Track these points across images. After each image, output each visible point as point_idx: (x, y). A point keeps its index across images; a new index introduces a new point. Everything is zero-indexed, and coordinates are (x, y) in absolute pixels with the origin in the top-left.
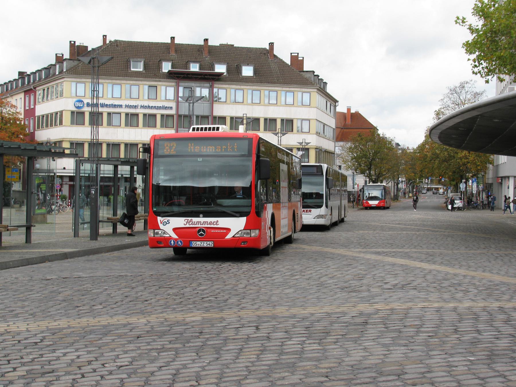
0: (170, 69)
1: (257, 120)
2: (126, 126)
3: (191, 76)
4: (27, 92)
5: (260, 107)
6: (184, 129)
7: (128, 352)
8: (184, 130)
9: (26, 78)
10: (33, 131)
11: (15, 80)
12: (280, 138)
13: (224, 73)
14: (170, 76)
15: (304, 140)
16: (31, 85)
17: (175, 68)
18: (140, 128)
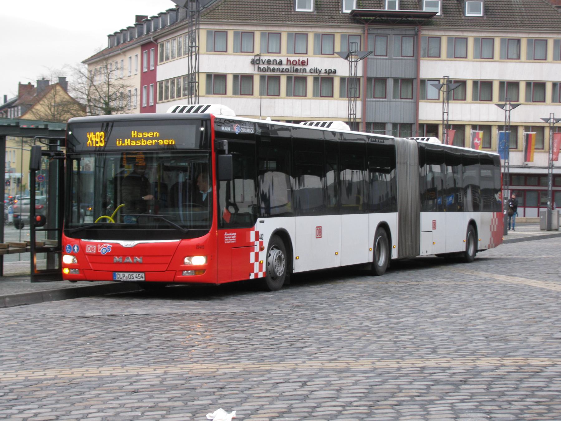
0: (354, 8)
1: (462, 83)
2: (287, 95)
3: (386, 18)
4: (146, 46)
5: (493, 63)
6: (374, 99)
7: (105, 411)
8: (375, 101)
9: (145, 26)
10: (153, 104)
11: (129, 28)
12: (508, 112)
13: (438, 13)
14: (354, 19)
15: (552, 115)
16: (151, 35)
17: (363, 7)
18: (308, 99)
